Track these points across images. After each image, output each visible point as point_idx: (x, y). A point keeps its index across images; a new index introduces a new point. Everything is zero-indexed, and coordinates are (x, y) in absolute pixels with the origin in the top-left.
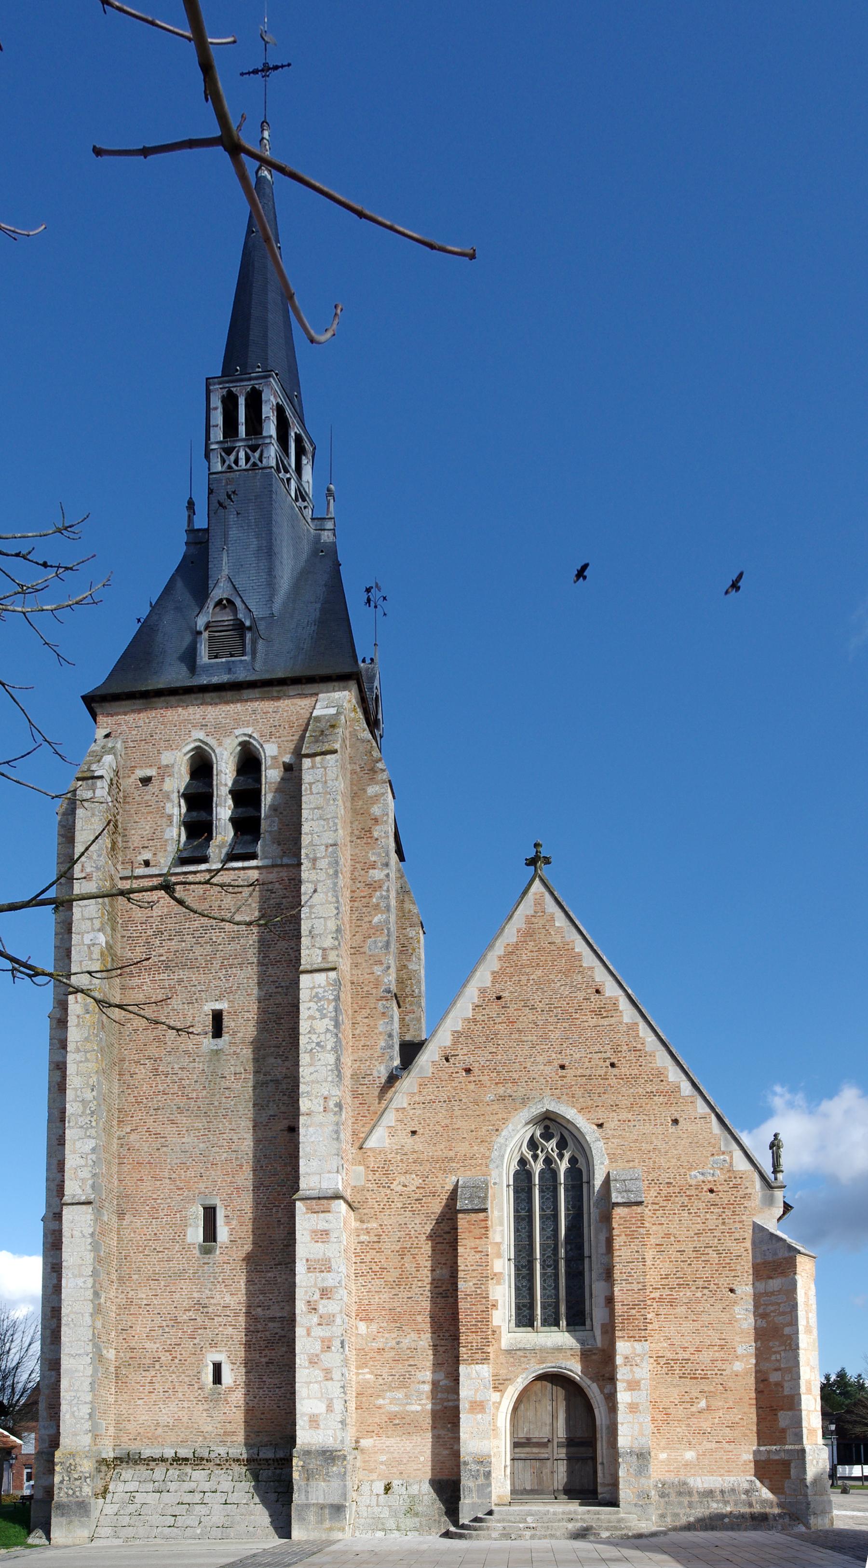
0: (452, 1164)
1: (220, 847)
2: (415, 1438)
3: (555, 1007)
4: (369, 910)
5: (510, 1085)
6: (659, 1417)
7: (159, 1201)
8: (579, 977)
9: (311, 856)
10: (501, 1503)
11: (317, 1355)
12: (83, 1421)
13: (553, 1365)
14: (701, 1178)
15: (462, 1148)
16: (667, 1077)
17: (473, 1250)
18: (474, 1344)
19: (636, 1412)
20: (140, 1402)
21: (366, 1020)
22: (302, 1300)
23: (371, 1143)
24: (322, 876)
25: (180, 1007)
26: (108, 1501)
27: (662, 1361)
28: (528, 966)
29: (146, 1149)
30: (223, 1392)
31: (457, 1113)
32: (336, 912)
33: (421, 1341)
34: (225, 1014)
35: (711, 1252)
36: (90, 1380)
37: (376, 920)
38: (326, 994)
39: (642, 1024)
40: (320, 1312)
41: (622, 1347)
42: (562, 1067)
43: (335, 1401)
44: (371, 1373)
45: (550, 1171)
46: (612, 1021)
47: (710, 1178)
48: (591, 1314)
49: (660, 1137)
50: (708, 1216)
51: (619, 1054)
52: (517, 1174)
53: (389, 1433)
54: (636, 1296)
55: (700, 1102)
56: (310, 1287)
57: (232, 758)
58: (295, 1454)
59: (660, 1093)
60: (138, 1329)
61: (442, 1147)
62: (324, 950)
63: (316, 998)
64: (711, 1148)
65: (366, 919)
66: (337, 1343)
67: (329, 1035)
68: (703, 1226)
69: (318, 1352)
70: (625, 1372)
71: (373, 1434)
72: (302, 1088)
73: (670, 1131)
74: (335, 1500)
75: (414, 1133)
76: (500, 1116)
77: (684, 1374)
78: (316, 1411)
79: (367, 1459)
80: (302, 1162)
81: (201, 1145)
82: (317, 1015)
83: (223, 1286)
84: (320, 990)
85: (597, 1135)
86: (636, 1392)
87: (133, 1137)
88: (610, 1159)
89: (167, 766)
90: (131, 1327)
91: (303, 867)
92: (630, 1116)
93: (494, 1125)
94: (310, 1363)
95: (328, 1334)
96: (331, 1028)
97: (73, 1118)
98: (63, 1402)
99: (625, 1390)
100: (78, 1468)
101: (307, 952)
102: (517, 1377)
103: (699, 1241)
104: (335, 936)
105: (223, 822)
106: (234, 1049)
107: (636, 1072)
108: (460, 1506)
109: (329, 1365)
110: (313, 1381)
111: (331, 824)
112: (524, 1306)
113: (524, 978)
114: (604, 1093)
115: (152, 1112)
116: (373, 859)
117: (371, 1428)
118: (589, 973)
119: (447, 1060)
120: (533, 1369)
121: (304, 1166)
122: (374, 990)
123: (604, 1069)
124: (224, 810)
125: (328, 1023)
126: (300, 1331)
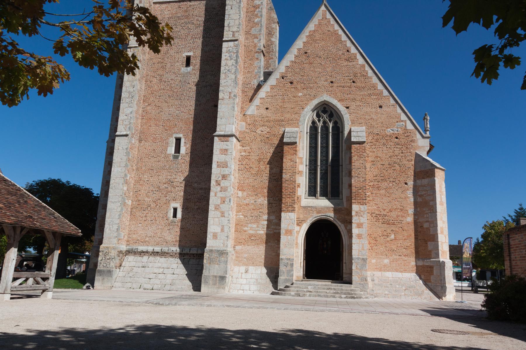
6: (372, 242)
8: (340, 45)
14: (392, 132)
15: (288, 116)
20: (140, 225)
26: (121, 270)
27: (374, 215)
33: (263, 201)
37: (256, 20)
39: (366, 65)
41: (355, 207)
42: (332, 82)
44: (243, 215)
45: (325, 127)
46: (354, 63)
47: (396, 132)
50: (395, 149)
52: (311, 127)
55: (391, 99)
58: (205, 251)
59: (374, 94)
62: (233, 32)
63: (229, 52)
65: (252, 20)
66: (227, 200)
67: (233, 67)
72: (221, 88)
74: (221, 274)
75: (267, 109)
76: (304, 103)
80: (218, 120)
81: (177, 112)
82: (229, 58)
84: (231, 48)
85: (346, 111)
87: (149, 108)
92: (361, 104)
100: (110, 254)
102: (307, 219)
106: (194, 72)
107: (364, 85)
113: (317, 45)
115: (158, 97)
117: (241, 241)
119: (283, 78)
125: (233, 62)
126: (212, 194)
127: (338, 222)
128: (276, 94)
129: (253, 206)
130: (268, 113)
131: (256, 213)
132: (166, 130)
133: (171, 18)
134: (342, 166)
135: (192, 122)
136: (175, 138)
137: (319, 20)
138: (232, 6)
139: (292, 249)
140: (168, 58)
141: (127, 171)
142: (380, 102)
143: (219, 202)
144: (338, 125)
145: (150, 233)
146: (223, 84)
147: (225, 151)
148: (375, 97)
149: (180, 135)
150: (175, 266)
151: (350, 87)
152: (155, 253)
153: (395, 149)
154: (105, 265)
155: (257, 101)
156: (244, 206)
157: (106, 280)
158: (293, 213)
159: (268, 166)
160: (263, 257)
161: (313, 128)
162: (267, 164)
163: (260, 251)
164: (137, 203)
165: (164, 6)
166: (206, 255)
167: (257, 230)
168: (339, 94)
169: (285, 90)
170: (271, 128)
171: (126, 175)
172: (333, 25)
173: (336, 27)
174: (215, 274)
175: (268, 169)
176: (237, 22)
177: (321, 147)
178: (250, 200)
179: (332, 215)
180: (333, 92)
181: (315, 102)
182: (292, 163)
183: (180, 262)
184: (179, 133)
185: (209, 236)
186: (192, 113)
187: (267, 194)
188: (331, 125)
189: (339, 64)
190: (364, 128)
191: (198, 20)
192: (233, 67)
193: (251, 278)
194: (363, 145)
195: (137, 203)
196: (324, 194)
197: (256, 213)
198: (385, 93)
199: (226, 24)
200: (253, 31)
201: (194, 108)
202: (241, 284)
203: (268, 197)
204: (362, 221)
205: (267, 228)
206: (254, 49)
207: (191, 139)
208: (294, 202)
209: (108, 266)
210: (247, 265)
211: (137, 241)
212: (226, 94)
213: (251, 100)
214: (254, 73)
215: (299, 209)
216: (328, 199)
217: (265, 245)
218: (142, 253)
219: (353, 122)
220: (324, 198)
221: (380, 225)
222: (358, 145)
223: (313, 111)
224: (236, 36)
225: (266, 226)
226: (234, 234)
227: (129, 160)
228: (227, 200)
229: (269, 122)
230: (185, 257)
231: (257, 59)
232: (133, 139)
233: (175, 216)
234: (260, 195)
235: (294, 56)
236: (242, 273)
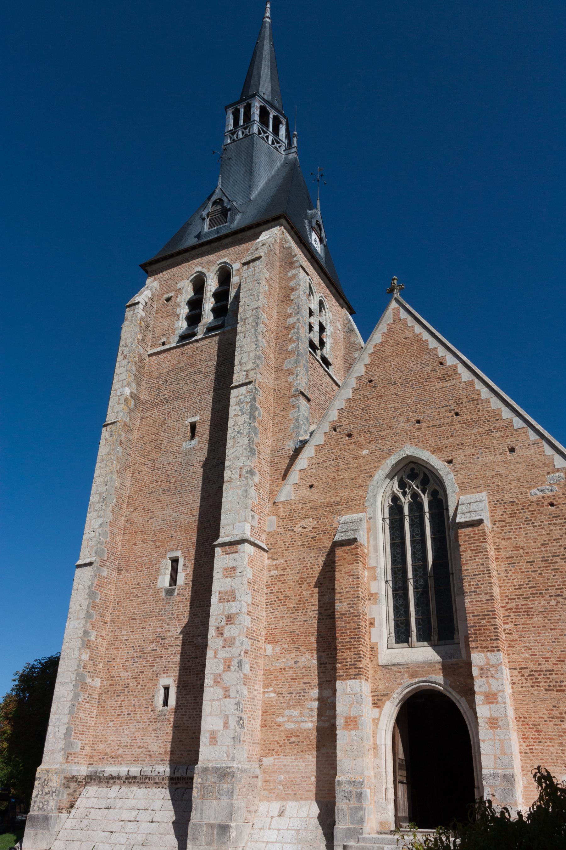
0: (338, 507)
1: (204, 325)
2: (307, 756)
3: (411, 381)
4: (286, 342)
5: (380, 441)
6: (531, 734)
7: (144, 559)
8: (427, 357)
9: (243, 318)
10: (383, 831)
11: (220, 675)
12: (60, 740)
13: (424, 679)
14: (540, 494)
15: (346, 493)
16: (501, 416)
17: (347, 575)
18: (349, 660)
19: (495, 728)
20: (111, 724)
21: (282, 413)
22: (213, 626)
23: (282, 497)
24: (249, 327)
25: (172, 424)
26: (71, 816)
27: (526, 672)
28: (390, 356)
29: (141, 522)
30: (167, 714)
31: (342, 467)
32: (255, 347)
33: (310, 660)
34: (197, 424)
35: (559, 560)
36: (69, 704)
37: (290, 347)
38: (246, 398)
39: (476, 381)
40: (225, 636)
41: (477, 658)
42: (418, 422)
43: (230, 717)
44: (275, 692)
45: (416, 505)
46: (454, 382)
47: (549, 494)
48: (457, 627)
49: (500, 464)
50: (552, 527)
51: (461, 406)
52: (391, 508)
53: (287, 751)
54: (485, 606)
55: (530, 432)
56: (220, 614)
57: (216, 276)
58: (196, 771)
59: (497, 429)
60: (118, 660)
61: (331, 494)
62: (247, 371)
63: (239, 403)
64: (546, 468)
65: (284, 348)
66: (235, 663)
67: (246, 425)
68: (548, 537)
69: (221, 672)
70: (481, 684)
71: (274, 753)
72: (227, 463)
73: (509, 458)
74: (221, 820)
75: (311, 486)
76: (372, 466)
77: (549, 686)
78: (215, 728)
79: (268, 778)
80: (223, 516)
81: (174, 514)
82: (240, 413)
83: (176, 621)
84: (242, 397)
85: (448, 469)
86: (494, 705)
87: (134, 514)
88: (460, 487)
89: (180, 289)
90: (114, 659)
91: (238, 325)
92: (473, 451)
93: (368, 473)
94: (215, 682)
95: (229, 656)
96: (247, 420)
97: (93, 506)
98: (50, 723)
99: (483, 704)
100: (50, 784)
101: (237, 374)
102: (392, 691)
103: (546, 551)
104: (254, 361)
105: (207, 311)
106: (200, 445)
107: (476, 416)
108: (335, 831)
109: (228, 684)
110: (216, 698)
111: (256, 296)
112: (402, 623)
113: (388, 365)
114: (451, 436)
115: (148, 495)
116: (290, 312)
117: (272, 747)
118: (434, 352)
119: (335, 430)
120: (406, 684)
121: (224, 520)
122: (288, 392)
123: (450, 419)
124: (209, 304)
125: (246, 417)
126: (210, 654)
127: (454, 693)
128: (325, 459)
129: (291, 673)
130: (314, 495)
131: (297, 686)
132: (157, 547)
133: (172, 371)
134: (452, 574)
135: (196, 528)
136: (170, 558)
137: (388, 325)
138: (244, 333)
139: (359, 760)
140: (164, 432)
141: (89, 626)
142: (510, 442)
143: (220, 668)
144: (439, 497)
145: (126, 740)
146: (230, 456)
147: (231, 571)
148: (498, 434)
149: (178, 554)
150: (157, 804)
151: (451, 424)
152: (131, 780)
153: (552, 527)
154: (41, 805)
155: (294, 476)
156: (275, 674)
157: (40, 835)
158: (358, 681)
159: (316, 590)
160: (313, 779)
161: (396, 509)
162: (315, 587)
163: (306, 765)
164: (110, 682)
165: (162, 356)
166: (197, 780)
167: (299, 722)
168: (431, 441)
169: (340, 450)
170: (318, 519)
171: (86, 633)
172: (412, 327)
173: (418, 329)
174: (212, 821)
175: (316, 596)
176: (252, 355)
177: (412, 542)
178: (287, 661)
179: (439, 678)
180: (421, 439)
181: (391, 461)
182: (351, 579)
183: (168, 796)
184: (176, 549)
185: (204, 739)
186: (197, 513)
187: (315, 645)
188: (425, 499)
189: (428, 388)
190: (484, 494)
191: (207, 366)
192: (246, 425)
193: (287, 829)
194: (480, 528)
195: (110, 682)
196: (425, 636)
197: (297, 686)
198: (518, 423)
199: (236, 361)
200: (287, 365)
201: (199, 504)
202: (267, 843)
203: (318, 651)
204: (494, 688)
205: (318, 715)
206: (287, 393)
207: (193, 557)
208: (359, 658)
209: (45, 807)
210: (283, 799)
211: (105, 757)
212: (234, 471)
213: (285, 476)
214: (289, 429)
215: (376, 672)
216: (431, 646)
217: (315, 753)
218: (111, 780)
219: (463, 488)
220: (426, 644)
221: (543, 694)
222: (470, 529)
223: (391, 476)
224: (251, 376)
225: (316, 712)
226: (259, 734)
227: (94, 606)
228: (235, 663)
229: (316, 509)
230: (178, 786)
231: (293, 406)
232: (105, 569)
233: (166, 703)
234: (302, 649)
235: (351, 390)
236: (272, 817)
